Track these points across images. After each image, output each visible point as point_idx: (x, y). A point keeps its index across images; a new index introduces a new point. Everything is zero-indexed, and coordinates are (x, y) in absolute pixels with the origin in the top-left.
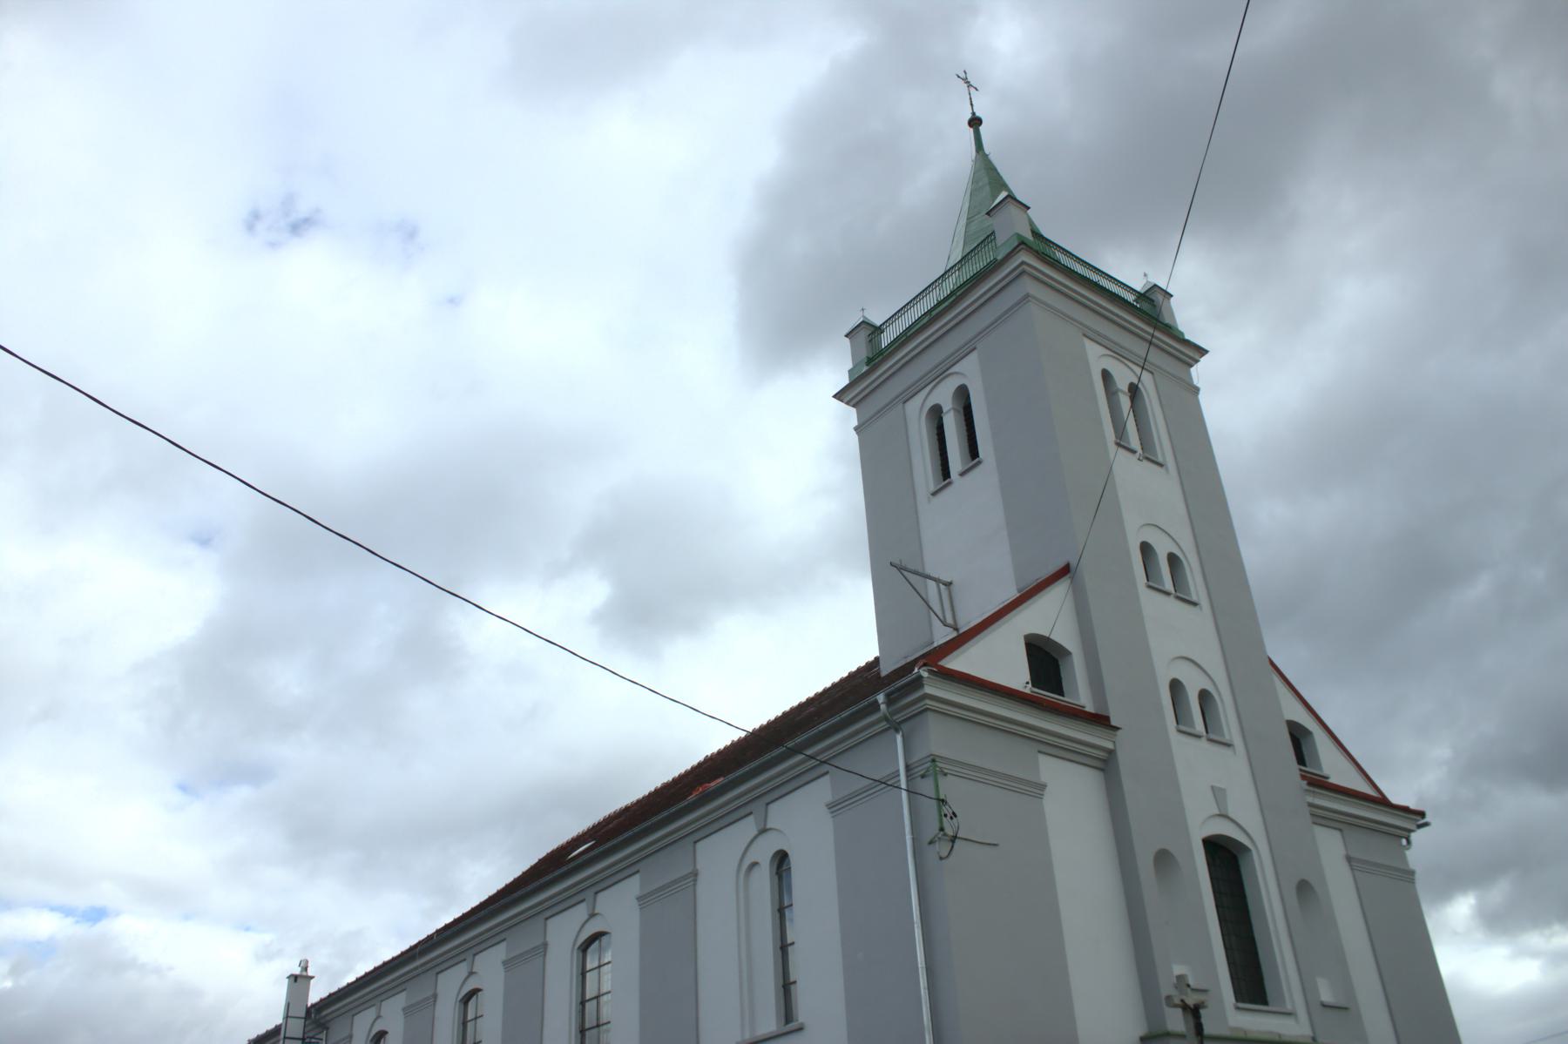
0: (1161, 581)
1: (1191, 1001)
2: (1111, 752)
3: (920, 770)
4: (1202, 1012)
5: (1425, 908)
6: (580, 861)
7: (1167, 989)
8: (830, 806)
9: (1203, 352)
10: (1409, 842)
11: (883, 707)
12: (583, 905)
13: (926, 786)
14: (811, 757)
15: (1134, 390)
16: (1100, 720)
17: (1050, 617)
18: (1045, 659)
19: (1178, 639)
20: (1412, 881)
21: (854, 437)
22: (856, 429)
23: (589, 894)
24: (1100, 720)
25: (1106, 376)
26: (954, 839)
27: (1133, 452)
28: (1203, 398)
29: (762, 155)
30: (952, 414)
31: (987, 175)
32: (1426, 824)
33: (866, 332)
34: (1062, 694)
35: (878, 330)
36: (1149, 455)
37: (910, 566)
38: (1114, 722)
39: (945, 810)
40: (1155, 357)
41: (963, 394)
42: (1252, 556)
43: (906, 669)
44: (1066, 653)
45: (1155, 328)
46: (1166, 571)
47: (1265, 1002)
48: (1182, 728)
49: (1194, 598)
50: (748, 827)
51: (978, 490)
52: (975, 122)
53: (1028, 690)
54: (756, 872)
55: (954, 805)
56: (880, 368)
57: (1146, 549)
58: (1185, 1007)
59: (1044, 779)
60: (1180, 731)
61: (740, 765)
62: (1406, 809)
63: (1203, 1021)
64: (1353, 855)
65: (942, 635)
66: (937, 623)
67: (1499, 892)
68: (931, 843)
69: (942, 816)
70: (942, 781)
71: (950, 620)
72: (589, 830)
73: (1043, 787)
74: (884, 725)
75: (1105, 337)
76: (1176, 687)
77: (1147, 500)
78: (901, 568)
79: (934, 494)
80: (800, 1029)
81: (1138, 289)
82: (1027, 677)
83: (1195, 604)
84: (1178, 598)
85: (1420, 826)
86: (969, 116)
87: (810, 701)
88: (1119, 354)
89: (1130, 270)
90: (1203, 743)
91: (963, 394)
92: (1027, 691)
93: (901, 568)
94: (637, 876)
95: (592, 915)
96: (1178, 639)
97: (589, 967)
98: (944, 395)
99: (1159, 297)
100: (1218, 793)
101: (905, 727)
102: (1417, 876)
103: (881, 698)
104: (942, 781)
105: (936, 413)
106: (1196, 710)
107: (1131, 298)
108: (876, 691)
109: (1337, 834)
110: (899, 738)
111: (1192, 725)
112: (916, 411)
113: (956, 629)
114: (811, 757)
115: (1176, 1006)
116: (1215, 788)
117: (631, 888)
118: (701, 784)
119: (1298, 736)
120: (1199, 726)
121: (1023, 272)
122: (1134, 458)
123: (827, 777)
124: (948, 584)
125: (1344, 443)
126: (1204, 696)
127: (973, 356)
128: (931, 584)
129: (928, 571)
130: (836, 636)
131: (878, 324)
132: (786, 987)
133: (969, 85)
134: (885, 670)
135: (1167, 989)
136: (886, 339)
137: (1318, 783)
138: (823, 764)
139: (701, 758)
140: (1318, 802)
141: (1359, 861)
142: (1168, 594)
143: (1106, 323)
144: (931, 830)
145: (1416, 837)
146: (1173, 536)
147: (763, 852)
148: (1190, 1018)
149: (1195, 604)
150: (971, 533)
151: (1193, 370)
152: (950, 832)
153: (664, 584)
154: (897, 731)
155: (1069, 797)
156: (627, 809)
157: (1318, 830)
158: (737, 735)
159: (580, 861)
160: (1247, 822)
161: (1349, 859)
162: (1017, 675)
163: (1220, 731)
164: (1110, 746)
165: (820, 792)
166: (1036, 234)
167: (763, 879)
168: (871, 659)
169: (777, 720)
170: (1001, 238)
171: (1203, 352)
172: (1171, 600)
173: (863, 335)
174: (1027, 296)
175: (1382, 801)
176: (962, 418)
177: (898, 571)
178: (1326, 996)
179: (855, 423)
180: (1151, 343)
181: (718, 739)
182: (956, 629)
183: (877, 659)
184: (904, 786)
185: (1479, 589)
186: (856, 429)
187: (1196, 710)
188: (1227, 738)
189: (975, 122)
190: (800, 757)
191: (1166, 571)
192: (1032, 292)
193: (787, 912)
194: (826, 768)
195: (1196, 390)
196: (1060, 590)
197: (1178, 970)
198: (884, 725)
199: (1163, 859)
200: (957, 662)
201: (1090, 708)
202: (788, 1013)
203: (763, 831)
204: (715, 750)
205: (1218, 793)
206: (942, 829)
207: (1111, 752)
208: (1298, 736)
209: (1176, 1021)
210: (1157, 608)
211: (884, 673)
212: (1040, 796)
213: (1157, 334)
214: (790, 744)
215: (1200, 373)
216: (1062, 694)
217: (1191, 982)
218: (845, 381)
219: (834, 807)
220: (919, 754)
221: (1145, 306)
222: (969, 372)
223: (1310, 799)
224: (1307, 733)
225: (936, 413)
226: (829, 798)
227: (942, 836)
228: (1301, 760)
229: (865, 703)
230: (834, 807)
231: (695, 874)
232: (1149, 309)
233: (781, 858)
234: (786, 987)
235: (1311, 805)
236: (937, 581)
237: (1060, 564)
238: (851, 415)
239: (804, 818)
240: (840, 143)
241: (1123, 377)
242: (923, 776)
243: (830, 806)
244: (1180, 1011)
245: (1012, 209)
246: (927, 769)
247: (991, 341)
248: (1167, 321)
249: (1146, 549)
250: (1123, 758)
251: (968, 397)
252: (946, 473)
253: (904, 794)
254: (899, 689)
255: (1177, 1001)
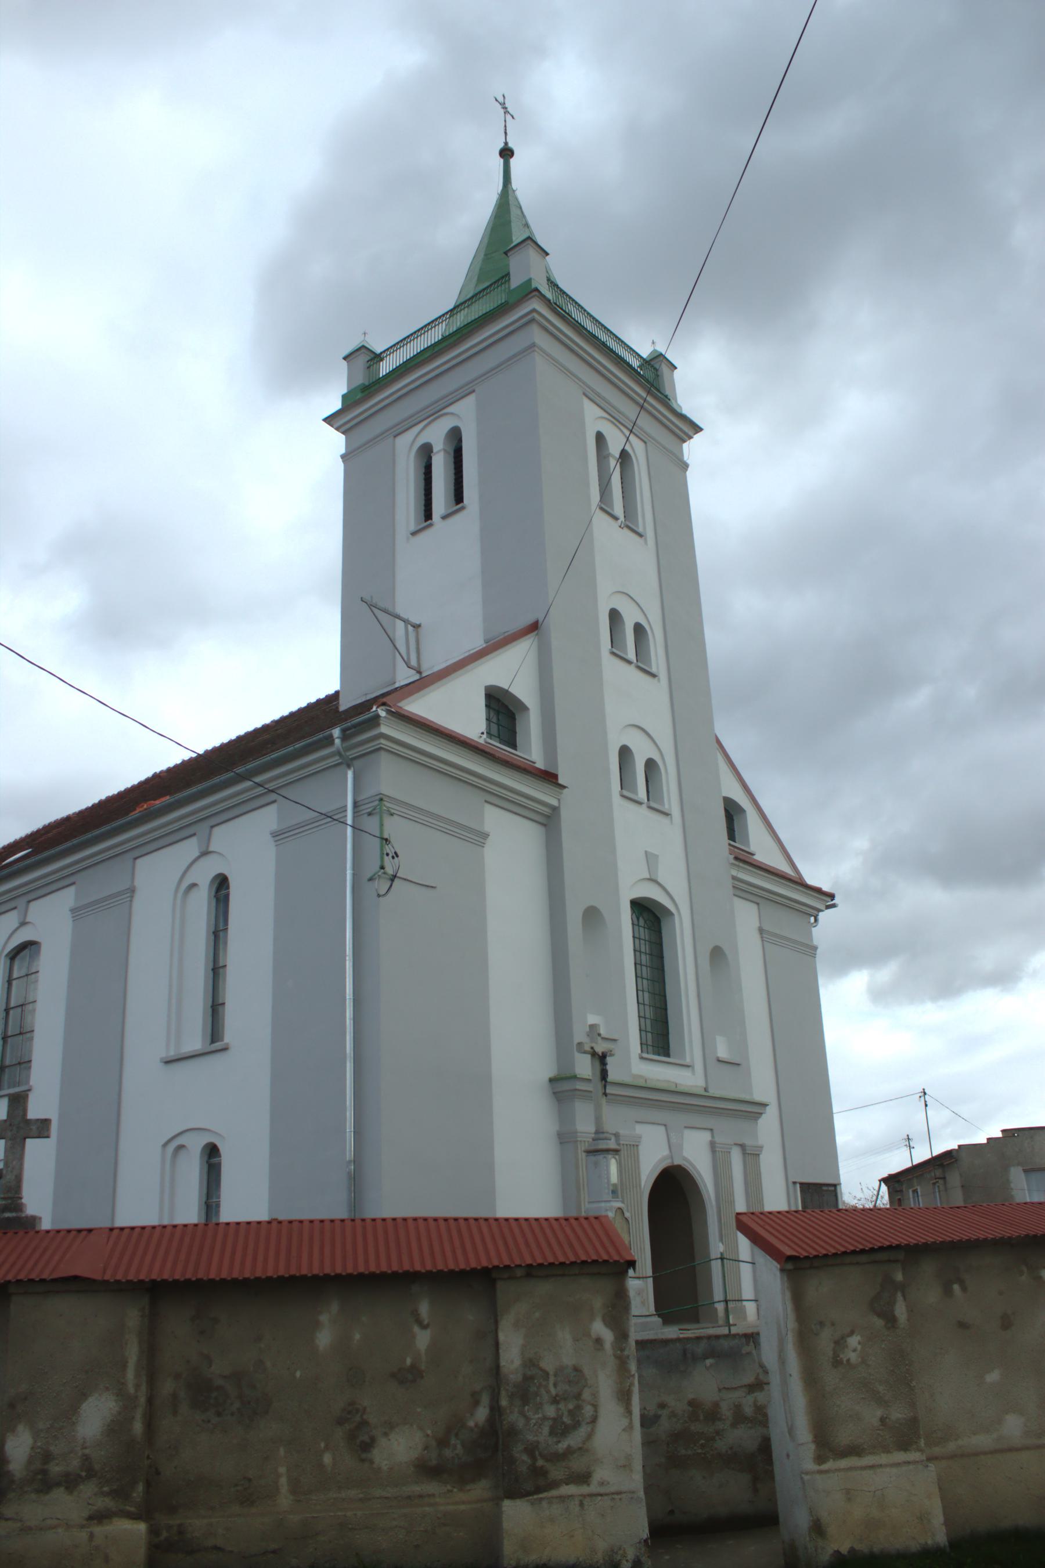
0: (624, 648)
1: (600, 1049)
2: (555, 809)
3: (368, 807)
4: (609, 1059)
5: (821, 981)
6: (15, 867)
7: (580, 1035)
8: (275, 835)
9: (697, 429)
10: (816, 920)
11: (337, 741)
12: (14, 913)
13: (371, 824)
14: (259, 785)
15: (624, 457)
16: (549, 777)
17: (513, 670)
18: (502, 708)
19: (632, 708)
20: (814, 956)
21: (340, 466)
22: (343, 457)
23: (21, 902)
24: (549, 777)
25: (600, 438)
26: (393, 878)
27: (616, 518)
28: (693, 477)
29: (302, 169)
30: (442, 454)
31: (506, 205)
32: (834, 906)
33: (364, 357)
34: (514, 746)
35: (377, 358)
36: (630, 524)
37: (381, 604)
38: (561, 781)
39: (388, 849)
40: (645, 423)
41: (455, 437)
42: (717, 641)
43: (365, 706)
44: (524, 708)
45: (649, 392)
46: (628, 639)
47: (668, 1055)
48: (625, 793)
49: (654, 670)
50: (190, 848)
51: (458, 536)
52: (506, 153)
53: (482, 740)
54: (194, 894)
55: (397, 845)
56: (373, 396)
57: (615, 616)
58: (594, 1054)
59: (487, 828)
60: (623, 796)
61: (188, 785)
62: (818, 891)
63: (608, 1067)
64: (766, 927)
65: (404, 676)
66: (401, 665)
67: (886, 973)
68: (370, 879)
69: (383, 854)
70: (388, 821)
71: (414, 662)
72: (28, 837)
73: (485, 836)
74: (336, 759)
75: (604, 399)
76: (625, 753)
77: (621, 567)
78: (372, 606)
79: (414, 534)
80: (225, 1049)
81: (645, 356)
82: (483, 726)
83: (654, 676)
84: (638, 667)
85: (828, 907)
86: (502, 145)
87: (265, 728)
88: (616, 420)
89: (641, 340)
90: (643, 810)
91: (455, 437)
92: (481, 741)
93: (372, 606)
94: (72, 889)
95: (23, 924)
96: (632, 708)
97: (15, 975)
98: (436, 435)
99: (665, 369)
100: (651, 859)
101: (357, 763)
102: (818, 951)
103: (336, 732)
104: (388, 821)
105: (426, 452)
106: (641, 778)
107: (635, 363)
108: (333, 725)
109: (754, 907)
110: (350, 774)
111: (635, 792)
112: (404, 451)
113: (419, 672)
114: (259, 785)
115: (585, 1052)
116: (646, 851)
117: (65, 899)
118: (146, 801)
119: (732, 813)
120: (642, 794)
121: (533, 320)
122: (615, 525)
123: (274, 807)
124: (417, 627)
125: (830, 545)
126: (651, 765)
127: (471, 400)
128: (400, 624)
129: (400, 610)
130: (301, 667)
131: (378, 351)
132: (216, 1009)
133: (506, 112)
134: (344, 705)
135: (580, 1035)
136: (385, 368)
137: (744, 859)
138: (270, 793)
139: (150, 774)
140: (742, 876)
141: (769, 933)
142: (629, 662)
143: (609, 386)
144: (371, 866)
145: (824, 916)
146: (643, 607)
147: (204, 874)
148: (597, 1064)
149: (654, 676)
150: (444, 576)
151: (685, 446)
152: (390, 870)
153: (135, 604)
154: (349, 766)
155: (510, 847)
156: (68, 819)
157: (736, 900)
158: (187, 755)
159: (15, 867)
160: (673, 890)
161: (761, 931)
162: (473, 723)
163: (661, 800)
164: (554, 802)
165: (265, 820)
166: (553, 284)
167: (201, 902)
168: (331, 691)
169: (231, 742)
170: (515, 282)
171: (697, 429)
172: (632, 667)
173: (362, 360)
174: (533, 345)
175: (799, 883)
176: (451, 460)
177: (368, 604)
178: (722, 1053)
179: (343, 451)
180: (642, 407)
181: (171, 757)
182: (419, 672)
183: (337, 693)
184: (349, 821)
185: (920, 699)
186: (343, 457)
187: (641, 778)
188: (666, 808)
189: (506, 153)
190: (248, 784)
191: (628, 639)
192: (537, 341)
193: (221, 934)
194: (273, 796)
195: (685, 466)
196: (525, 647)
197: (592, 1019)
198: (336, 759)
199: (592, 915)
200: (417, 706)
201: (540, 765)
202: (215, 1030)
203: (205, 853)
204: (164, 767)
205: (651, 859)
206: (382, 868)
207: (555, 809)
208: (732, 813)
209: (584, 1066)
210: (617, 675)
211: (342, 708)
212: (482, 845)
213: (649, 399)
214: (240, 770)
215: (693, 450)
216: (514, 746)
217: (602, 1032)
218: (338, 405)
219: (277, 835)
220: (368, 793)
221: (649, 374)
222: (465, 414)
223: (734, 873)
224: (741, 811)
225: (426, 452)
226: (274, 827)
227: (380, 874)
228: (731, 835)
229: (321, 736)
230: (277, 835)
231: (132, 890)
232: (651, 377)
233: (221, 883)
234: (216, 1009)
235: (734, 878)
236: (406, 622)
237: (529, 620)
238: (336, 441)
239: (247, 844)
240: (378, 161)
241: (615, 443)
242: (370, 814)
243: (275, 835)
244: (589, 1056)
245: (532, 253)
246: (373, 808)
247: (486, 384)
248: (667, 393)
249: (615, 616)
250: (565, 814)
251: (460, 440)
252: (428, 515)
253: (349, 830)
254: (354, 726)
255: (587, 1048)
